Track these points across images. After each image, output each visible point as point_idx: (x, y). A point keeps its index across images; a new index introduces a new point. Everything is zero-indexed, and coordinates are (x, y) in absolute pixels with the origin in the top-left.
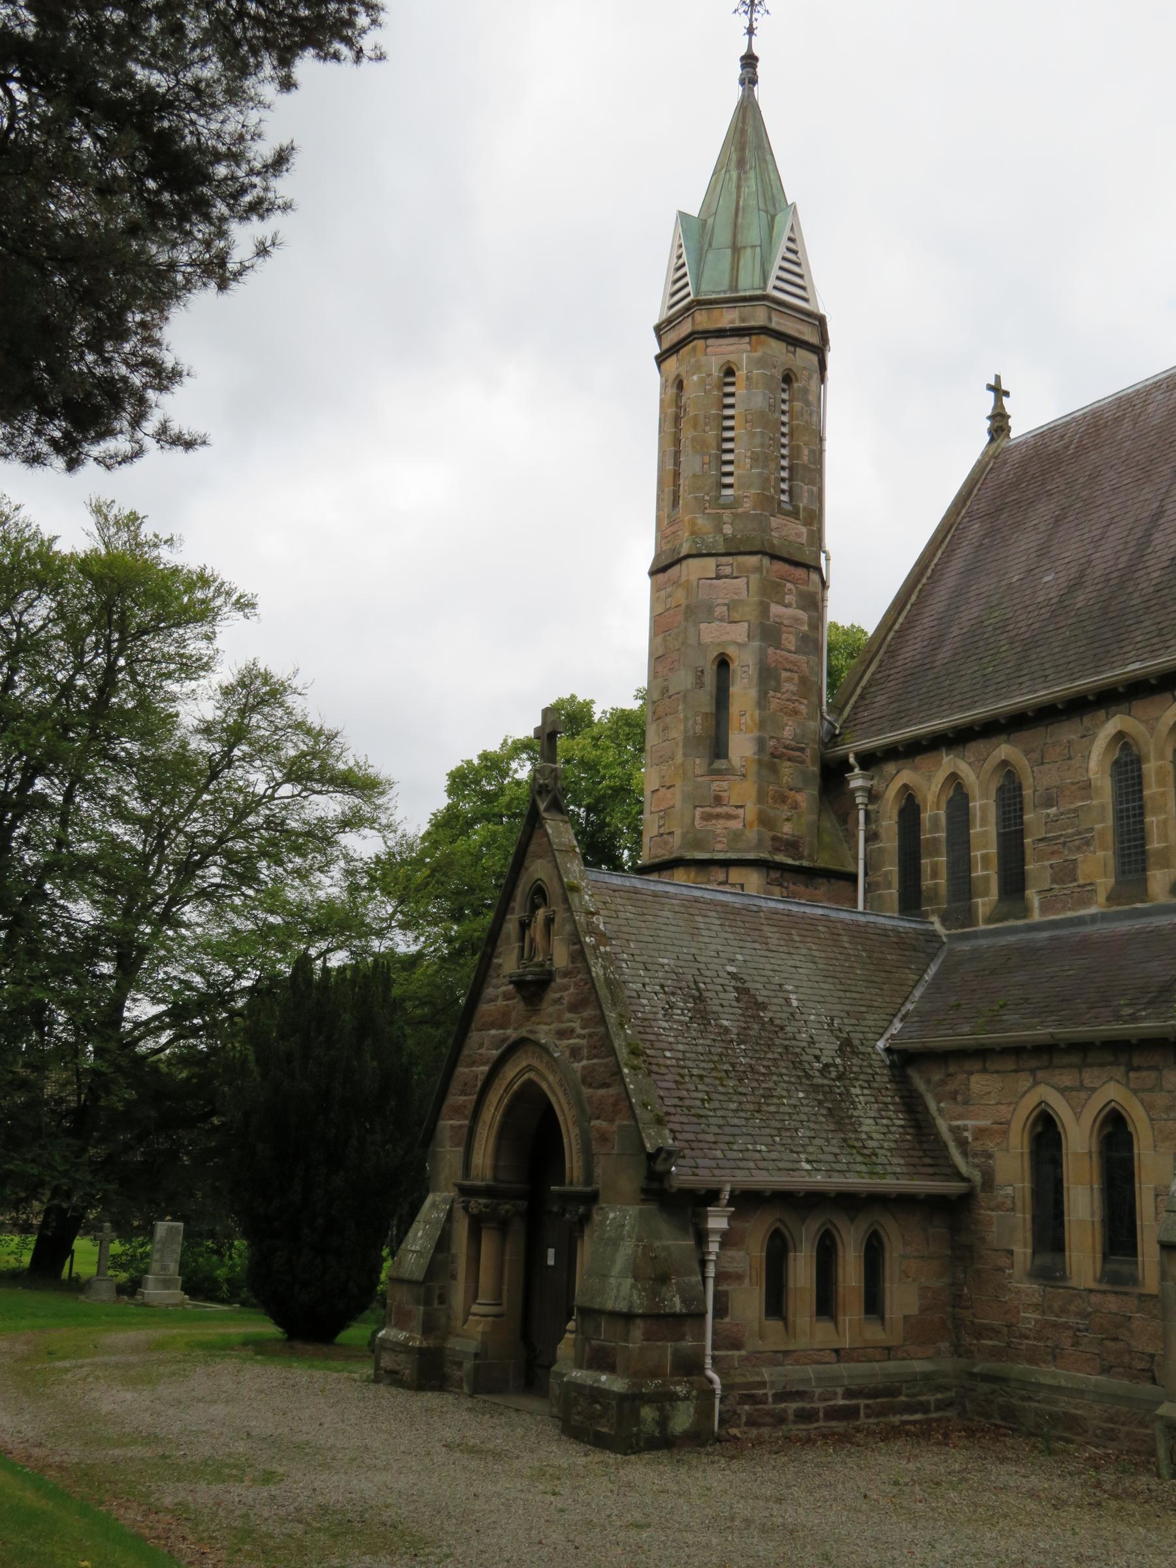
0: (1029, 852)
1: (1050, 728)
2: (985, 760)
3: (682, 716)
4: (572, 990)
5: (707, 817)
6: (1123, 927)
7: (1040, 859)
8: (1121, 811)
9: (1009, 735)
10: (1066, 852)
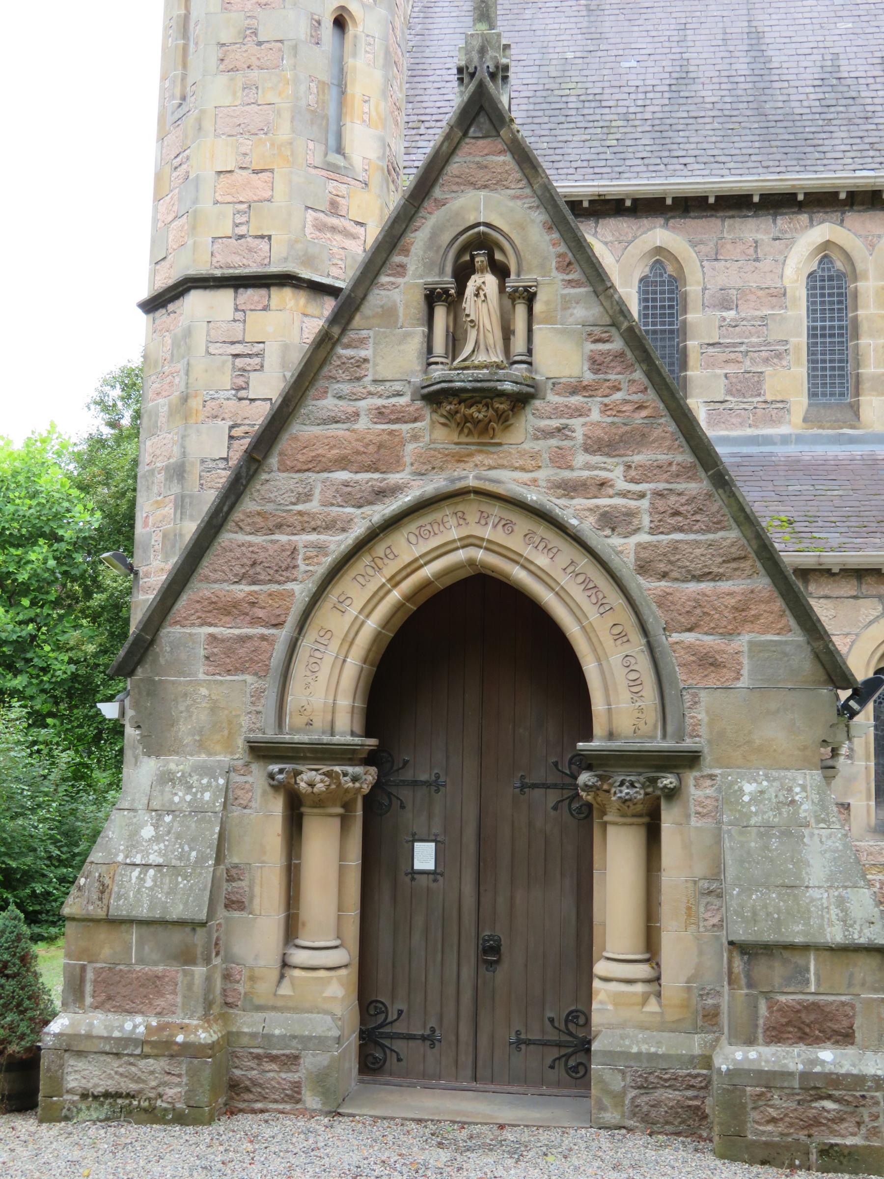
0: (693, 358)
1: (727, 222)
2: (630, 243)
3: (289, 75)
4: (595, 415)
5: (321, 227)
6: (820, 450)
7: (711, 365)
8: (814, 328)
9: (667, 220)
10: (748, 362)
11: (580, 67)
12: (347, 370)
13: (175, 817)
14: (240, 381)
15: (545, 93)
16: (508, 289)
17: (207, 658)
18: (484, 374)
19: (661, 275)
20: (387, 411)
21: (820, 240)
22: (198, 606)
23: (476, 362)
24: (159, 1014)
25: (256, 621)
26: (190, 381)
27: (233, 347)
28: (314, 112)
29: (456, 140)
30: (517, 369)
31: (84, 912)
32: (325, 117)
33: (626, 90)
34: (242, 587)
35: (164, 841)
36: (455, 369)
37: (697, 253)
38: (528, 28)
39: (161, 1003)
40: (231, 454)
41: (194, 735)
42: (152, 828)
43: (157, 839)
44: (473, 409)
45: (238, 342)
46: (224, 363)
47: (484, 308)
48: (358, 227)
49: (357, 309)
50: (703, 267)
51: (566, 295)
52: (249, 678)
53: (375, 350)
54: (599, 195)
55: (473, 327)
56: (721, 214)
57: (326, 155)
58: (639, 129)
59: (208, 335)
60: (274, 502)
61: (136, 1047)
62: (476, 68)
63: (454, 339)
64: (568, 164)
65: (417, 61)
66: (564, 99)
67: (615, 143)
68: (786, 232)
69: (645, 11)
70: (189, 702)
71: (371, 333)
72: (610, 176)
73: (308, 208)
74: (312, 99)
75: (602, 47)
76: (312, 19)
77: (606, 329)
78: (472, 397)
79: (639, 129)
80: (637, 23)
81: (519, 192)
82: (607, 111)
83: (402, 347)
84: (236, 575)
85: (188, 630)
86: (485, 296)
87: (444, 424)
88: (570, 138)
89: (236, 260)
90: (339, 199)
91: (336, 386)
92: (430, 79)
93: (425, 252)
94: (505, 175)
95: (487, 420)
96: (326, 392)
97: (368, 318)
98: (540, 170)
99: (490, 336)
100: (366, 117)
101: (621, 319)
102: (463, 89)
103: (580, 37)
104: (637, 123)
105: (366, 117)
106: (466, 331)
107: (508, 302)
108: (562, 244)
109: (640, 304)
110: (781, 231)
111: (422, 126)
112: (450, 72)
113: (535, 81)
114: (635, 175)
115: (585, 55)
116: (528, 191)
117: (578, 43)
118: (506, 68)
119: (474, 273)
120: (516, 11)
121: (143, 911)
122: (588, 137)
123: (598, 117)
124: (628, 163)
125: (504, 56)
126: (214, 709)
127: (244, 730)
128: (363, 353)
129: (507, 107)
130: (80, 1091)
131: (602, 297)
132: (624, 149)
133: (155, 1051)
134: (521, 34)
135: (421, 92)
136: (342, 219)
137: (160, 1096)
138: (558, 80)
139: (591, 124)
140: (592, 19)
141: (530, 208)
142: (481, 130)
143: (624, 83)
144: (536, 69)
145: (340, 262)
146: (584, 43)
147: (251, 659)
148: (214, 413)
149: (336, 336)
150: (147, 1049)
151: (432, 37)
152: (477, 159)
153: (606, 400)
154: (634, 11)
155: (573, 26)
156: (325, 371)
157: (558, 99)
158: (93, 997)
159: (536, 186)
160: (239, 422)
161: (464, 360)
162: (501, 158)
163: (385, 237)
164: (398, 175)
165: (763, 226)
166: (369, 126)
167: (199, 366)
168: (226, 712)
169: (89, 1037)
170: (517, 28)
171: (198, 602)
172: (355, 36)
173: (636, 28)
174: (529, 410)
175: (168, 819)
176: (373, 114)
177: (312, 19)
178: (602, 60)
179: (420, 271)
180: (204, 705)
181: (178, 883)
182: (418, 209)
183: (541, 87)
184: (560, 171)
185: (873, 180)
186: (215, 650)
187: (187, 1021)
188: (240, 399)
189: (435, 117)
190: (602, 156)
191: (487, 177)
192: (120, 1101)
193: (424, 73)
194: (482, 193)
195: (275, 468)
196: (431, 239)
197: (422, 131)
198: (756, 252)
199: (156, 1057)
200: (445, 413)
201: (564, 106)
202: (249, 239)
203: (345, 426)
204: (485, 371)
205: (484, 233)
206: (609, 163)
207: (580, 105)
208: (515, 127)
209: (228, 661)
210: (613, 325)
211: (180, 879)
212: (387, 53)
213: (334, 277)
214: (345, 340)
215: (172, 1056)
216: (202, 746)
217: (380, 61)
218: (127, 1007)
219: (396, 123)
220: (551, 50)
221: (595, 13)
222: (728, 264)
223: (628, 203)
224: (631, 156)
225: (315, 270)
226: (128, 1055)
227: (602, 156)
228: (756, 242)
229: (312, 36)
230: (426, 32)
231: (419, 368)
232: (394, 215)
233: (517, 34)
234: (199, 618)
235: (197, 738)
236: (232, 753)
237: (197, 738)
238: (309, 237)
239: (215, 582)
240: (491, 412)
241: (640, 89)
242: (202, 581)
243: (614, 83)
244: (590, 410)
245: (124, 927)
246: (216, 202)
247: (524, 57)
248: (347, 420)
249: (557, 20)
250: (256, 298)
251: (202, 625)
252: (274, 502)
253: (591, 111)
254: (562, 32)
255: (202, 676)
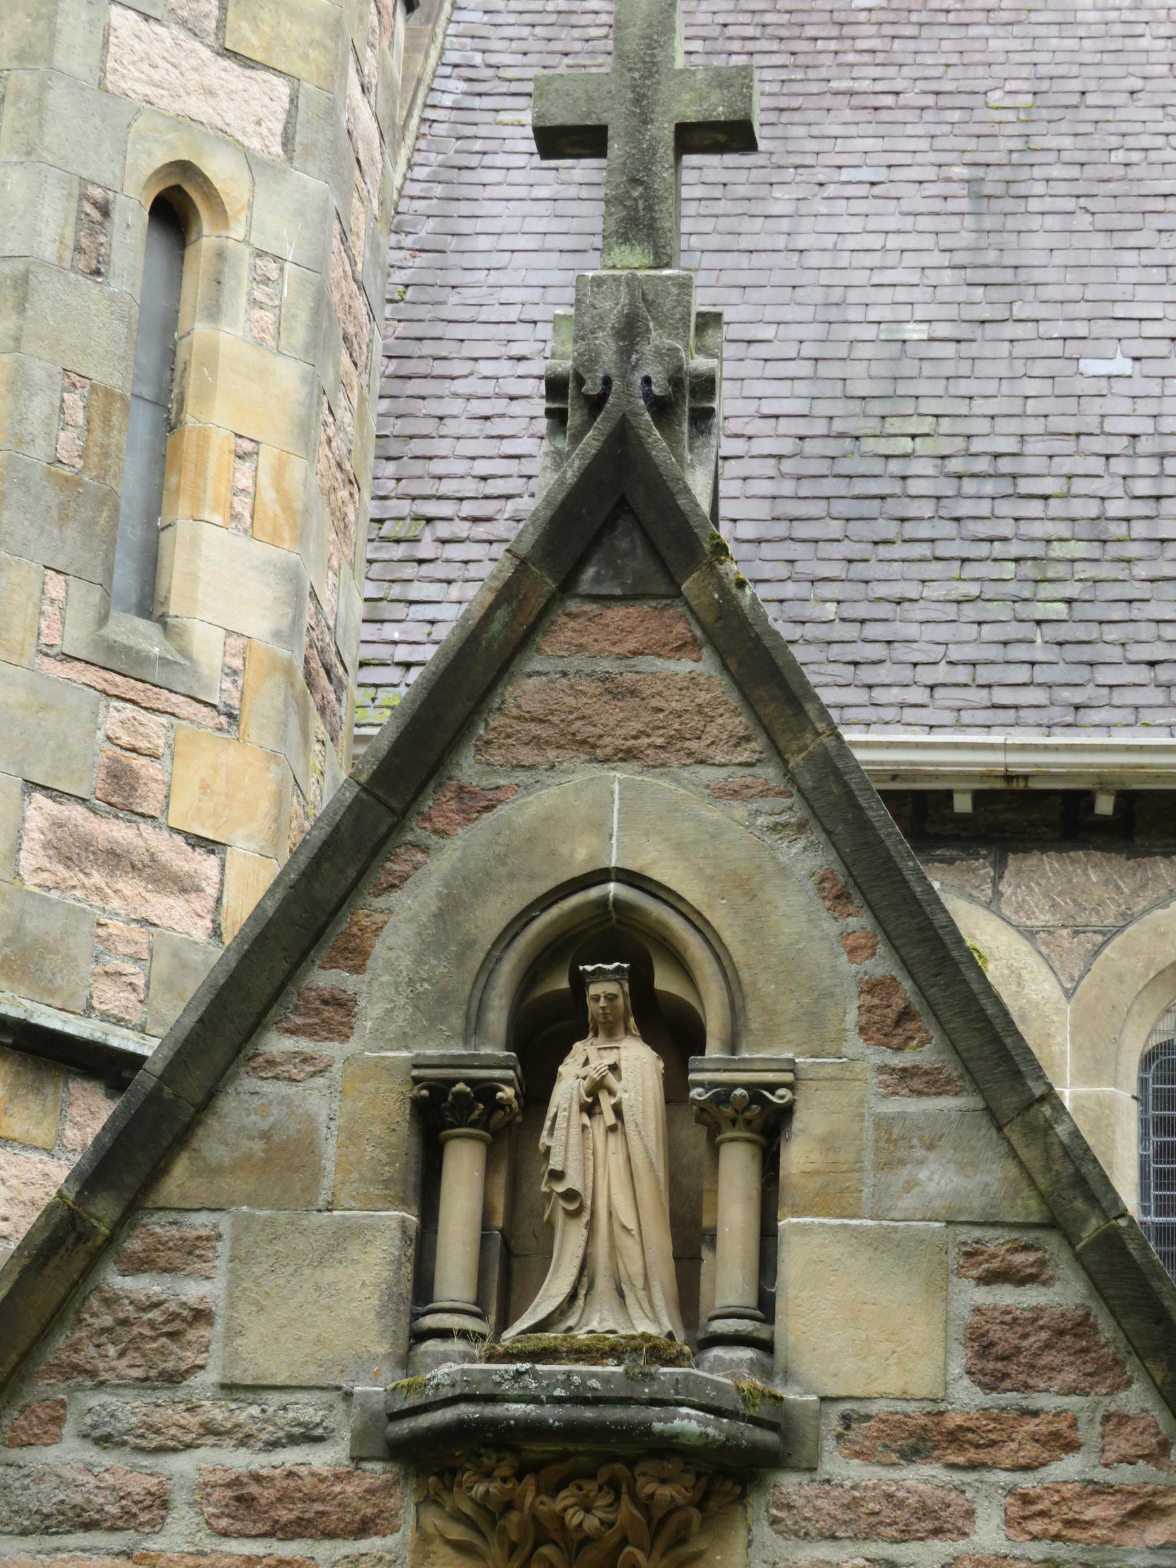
2: (1109, 934)
11: (948, 369)
12: (135, 1344)
15: (832, 447)
16: (695, 1093)
18: (606, 1379)
20: (266, 1494)
23: (581, 1335)
28: (71, 483)
29: (536, 604)
30: (720, 1364)
32: (108, 500)
33: (1098, 445)
36: (509, 1356)
38: (780, 242)
44: (566, 1498)
47: (612, 1153)
48: (199, 855)
49: (182, 1139)
51: (891, 1119)
53: (235, 1278)
54: (1009, 777)
55: (575, 1214)
57: (103, 619)
58: (1141, 571)
62: (607, 381)
63: (508, 1253)
64: (906, 674)
65: (417, 330)
66: (895, 467)
67: (1061, 609)
69: (1159, 204)
71: (224, 1222)
72: (1044, 716)
73: (32, 786)
74: (68, 442)
75: (1019, 311)
76: (84, 197)
77: (1028, 1237)
78: (562, 1457)
79: (1141, 571)
80: (1132, 240)
81: (740, 777)
82: (1035, 508)
83: (328, 1275)
86: (617, 1110)
87: (460, 1547)
88: (912, 590)
90: (138, 762)
91: (94, 1400)
92: (459, 386)
93: (419, 960)
94: (696, 721)
95: (611, 1536)
96: (58, 1421)
97: (216, 1171)
98: (809, 707)
99: (629, 1245)
100: (242, 505)
101: (1080, 1204)
102: (563, 444)
103: (947, 276)
104: (1134, 550)
105: (242, 505)
106: (550, 1226)
107: (694, 1135)
108: (881, 949)
109: (1144, 1138)
111: (428, 535)
112: (523, 368)
113: (801, 407)
114: (1127, 715)
115: (964, 331)
116: (770, 773)
117: (944, 294)
118: (706, 385)
119: (582, 1036)
120: (742, 191)
122: (973, 590)
123: (1005, 528)
124: (1106, 675)
125: (701, 350)
128: (193, 1291)
129: (706, 507)
131: (1014, 1134)
132: (1092, 632)
134: (759, 260)
135: (428, 427)
136: (146, 827)
138: (876, 408)
139: (983, 550)
140: (988, 223)
141: (775, 828)
142: (618, 574)
143: (1092, 424)
144: (805, 368)
145: (129, 968)
146: (963, 294)
149: (104, 1230)
151: (467, 260)
152: (605, 665)
153: (1027, 1482)
154: (1123, 203)
155: (927, 241)
156: (59, 1348)
157: (877, 466)
159: (795, 760)
161: (541, 1326)
162: (684, 666)
163: (283, 908)
164: (340, 687)
166: (250, 533)
170: (744, 243)
172: (220, 255)
173: (1129, 257)
174: (759, 1508)
176: (268, 494)
177: (84, 197)
178: (1020, 349)
179: (401, 1019)
182: (400, 818)
183: (820, 427)
184: (879, 695)
189: (468, 509)
190: (1019, 652)
191: (636, 725)
193: (440, 368)
194: (618, 776)
196: (440, 916)
197: (426, 549)
200: (467, 1508)
201: (895, 487)
203: (117, 1541)
204: (611, 1368)
205: (620, 905)
206: (1041, 673)
207: (947, 487)
208: (731, 569)
210: (1051, 1224)
212: (321, 305)
213: (105, 1017)
214: (134, 1245)
217: (299, 335)
219: (342, 527)
220: (854, 314)
221: (997, 205)
223: (1105, 805)
224: (1114, 653)
225: (47, 992)
227: (1019, 652)
229: (79, 249)
230: (453, 243)
231: (382, 1348)
232: (320, 836)
233: (744, 260)
238: (31, 882)
240: (626, 1507)
241: (1144, 446)
243: (1056, 424)
244: (970, 1514)
247: (768, 332)
248: (126, 1520)
249: (873, 223)
253: (984, 508)
254: (893, 258)
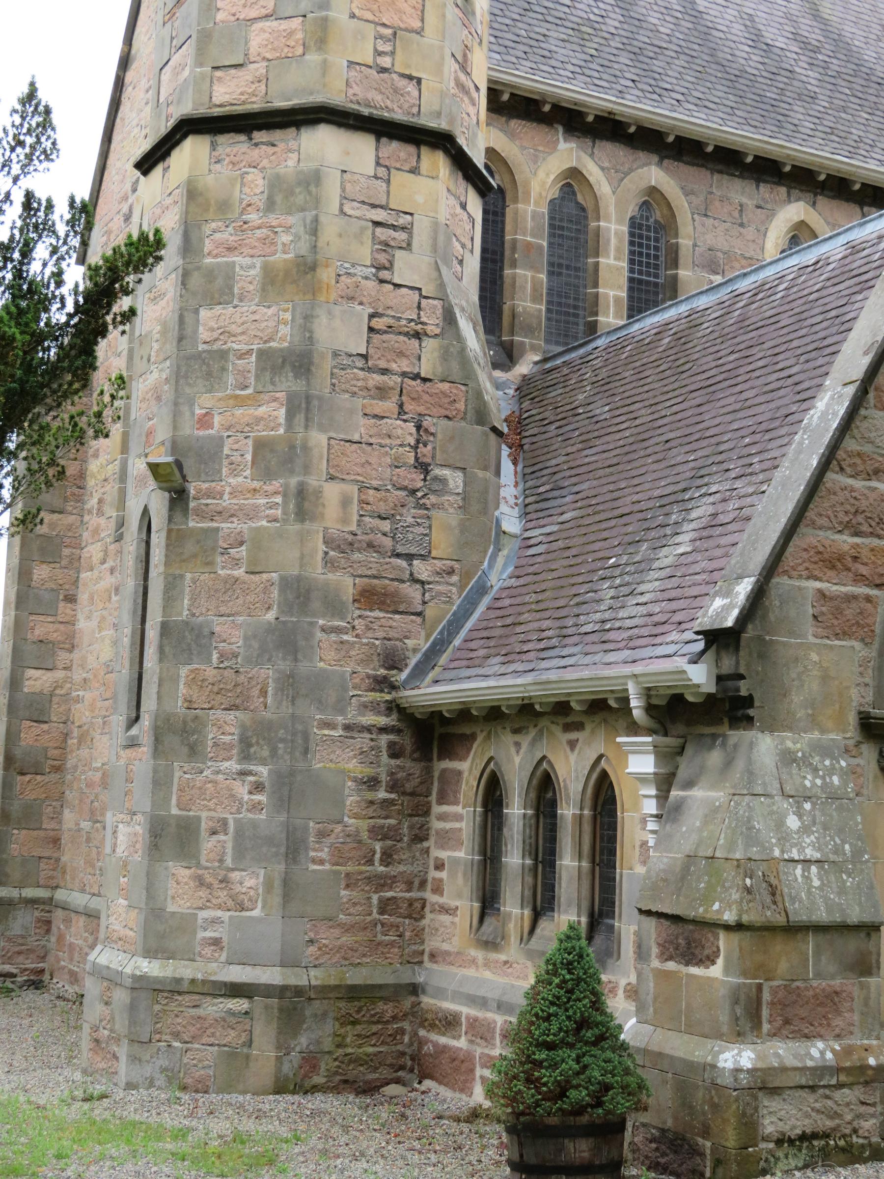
1: (716, 176)
2: (626, 174)
13: (814, 804)
14: (382, 258)
17: (815, 617)
19: (647, 219)
21: (796, 219)
22: (805, 555)
24: (838, 1037)
25: (859, 579)
26: (319, 244)
27: (373, 211)
31: (763, 919)
34: (845, 537)
35: (813, 832)
37: (690, 203)
39: (838, 1022)
40: (371, 351)
41: (806, 709)
42: (795, 818)
43: (805, 830)
45: (382, 207)
46: (363, 229)
50: (694, 220)
52: (857, 645)
56: (710, 166)
59: (343, 189)
60: (872, 443)
61: (832, 1076)
68: (767, 202)
70: (801, 669)
84: (841, 523)
85: (797, 583)
89: (378, 99)
110: (763, 199)
121: (822, 915)
126: (825, 678)
127: (854, 704)
130: (776, 1136)
133: (851, 1079)
137: (855, 1131)
147: (857, 623)
148: (350, 292)
150: (843, 1078)
158: (770, 1022)
160: (380, 310)
165: (747, 190)
167: (331, 228)
168: (836, 682)
169: (784, 1069)
171: (805, 550)
175: (807, 806)
180: (815, 673)
181: (844, 882)
185: (854, 169)
186: (824, 609)
187: (866, 1042)
188: (382, 281)
192: (815, 1143)
195: (872, 404)
198: (741, 216)
199: (850, 1086)
202: (394, 76)
209: (836, 622)
211: (845, 877)
215: (866, 1083)
216: (814, 723)
218: (806, 1031)
222: (716, 223)
226: (824, 1087)
228: (741, 206)
234: (807, 569)
235: (810, 712)
236: (844, 731)
237: (810, 712)
239: (820, 528)
242: (807, 526)
245: (799, 936)
246: (353, 16)
250: (402, 155)
251: (808, 578)
252: (872, 443)
255: (812, 639)
